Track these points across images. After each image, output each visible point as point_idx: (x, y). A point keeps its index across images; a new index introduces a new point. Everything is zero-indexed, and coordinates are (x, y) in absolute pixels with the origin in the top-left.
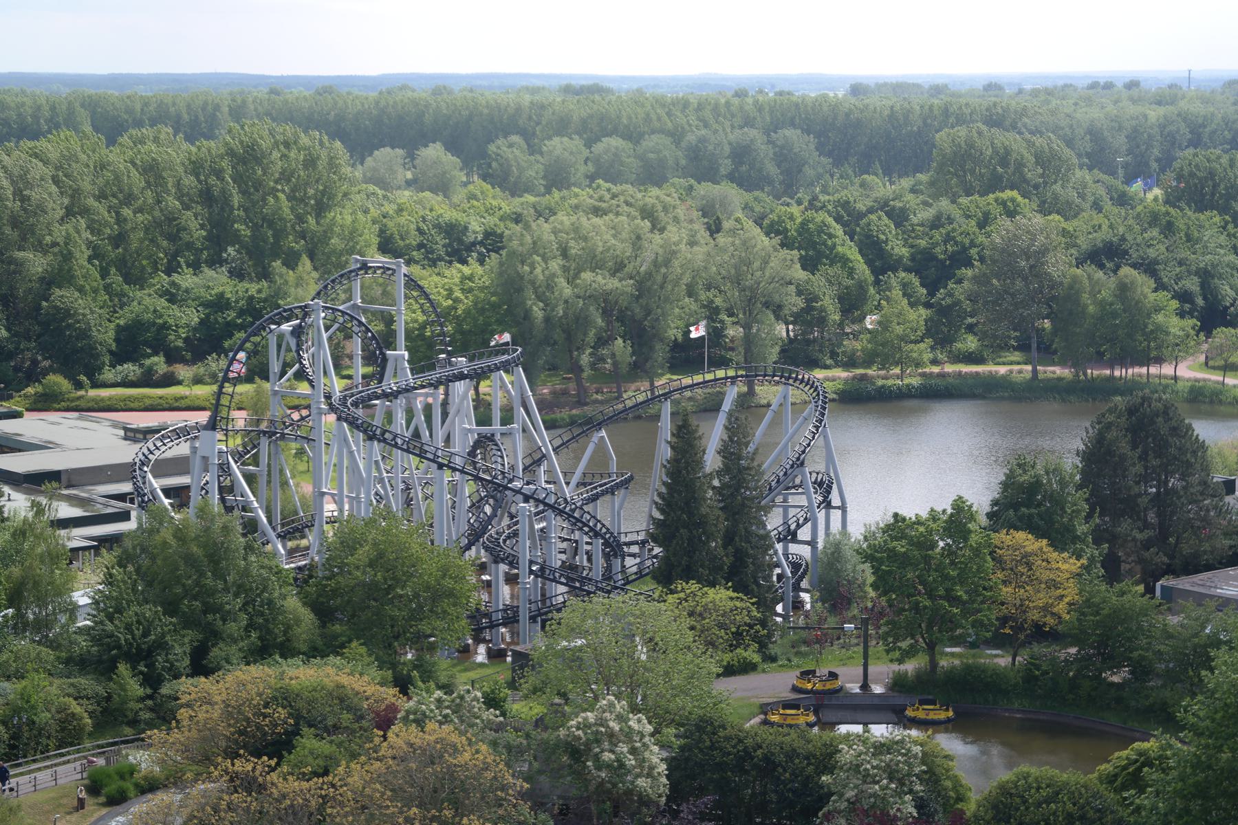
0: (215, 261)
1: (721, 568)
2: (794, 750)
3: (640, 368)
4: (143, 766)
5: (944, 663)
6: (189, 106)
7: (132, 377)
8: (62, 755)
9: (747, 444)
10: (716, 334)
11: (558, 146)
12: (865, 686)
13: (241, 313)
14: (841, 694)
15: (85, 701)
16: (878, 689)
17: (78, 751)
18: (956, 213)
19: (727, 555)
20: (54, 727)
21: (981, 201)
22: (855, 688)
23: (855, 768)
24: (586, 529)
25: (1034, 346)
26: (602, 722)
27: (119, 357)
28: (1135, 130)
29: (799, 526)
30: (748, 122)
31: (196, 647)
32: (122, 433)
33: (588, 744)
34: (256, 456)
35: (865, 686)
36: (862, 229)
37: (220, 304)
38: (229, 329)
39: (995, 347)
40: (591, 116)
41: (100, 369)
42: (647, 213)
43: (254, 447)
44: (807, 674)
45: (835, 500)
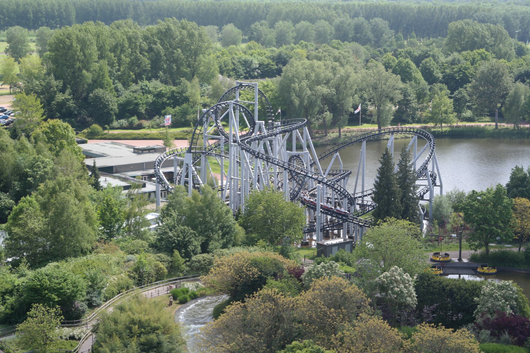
0: (157, 77)
1: (400, 212)
2: (460, 287)
3: (335, 123)
4: (190, 289)
5: (492, 250)
6: (116, 5)
7: (124, 125)
8: (157, 284)
9: (409, 161)
10: (364, 111)
11: (280, 25)
12: (460, 259)
13: (169, 98)
14: (451, 262)
15: (164, 263)
16: (465, 260)
17: (163, 283)
18: (461, 58)
19: (402, 206)
20: (153, 273)
21: (472, 53)
22: (456, 260)
23: (491, 295)
24: (339, 193)
25: (497, 114)
26: (392, 276)
27: (119, 117)
28: (523, 18)
29: (424, 193)
30: (356, 15)
31: (203, 243)
32: (132, 150)
33: (388, 284)
34: (199, 162)
35: (460, 259)
36: (423, 64)
37: (160, 95)
38: (164, 105)
39: (479, 114)
40: (290, 11)
41: (112, 121)
42: (336, 59)
43: (198, 158)
44: (436, 254)
45: (438, 182)
